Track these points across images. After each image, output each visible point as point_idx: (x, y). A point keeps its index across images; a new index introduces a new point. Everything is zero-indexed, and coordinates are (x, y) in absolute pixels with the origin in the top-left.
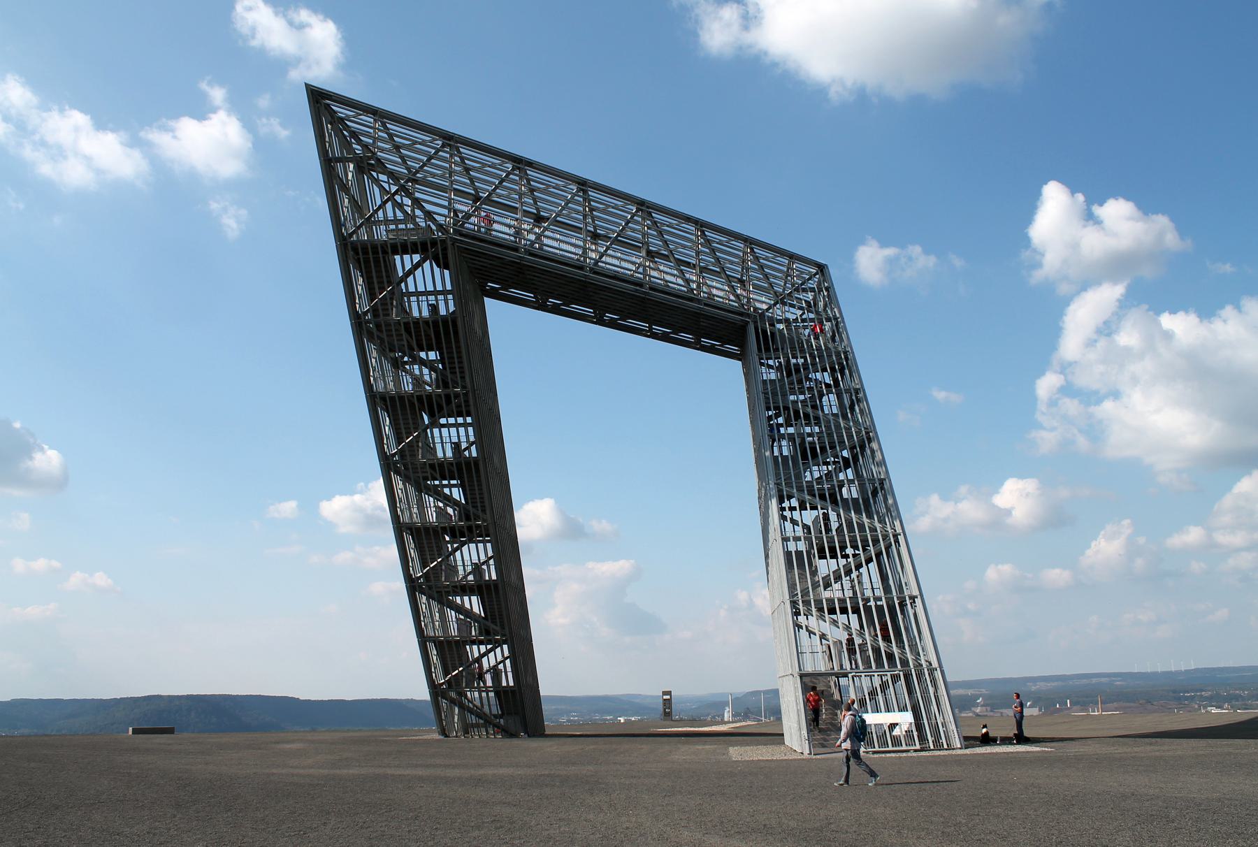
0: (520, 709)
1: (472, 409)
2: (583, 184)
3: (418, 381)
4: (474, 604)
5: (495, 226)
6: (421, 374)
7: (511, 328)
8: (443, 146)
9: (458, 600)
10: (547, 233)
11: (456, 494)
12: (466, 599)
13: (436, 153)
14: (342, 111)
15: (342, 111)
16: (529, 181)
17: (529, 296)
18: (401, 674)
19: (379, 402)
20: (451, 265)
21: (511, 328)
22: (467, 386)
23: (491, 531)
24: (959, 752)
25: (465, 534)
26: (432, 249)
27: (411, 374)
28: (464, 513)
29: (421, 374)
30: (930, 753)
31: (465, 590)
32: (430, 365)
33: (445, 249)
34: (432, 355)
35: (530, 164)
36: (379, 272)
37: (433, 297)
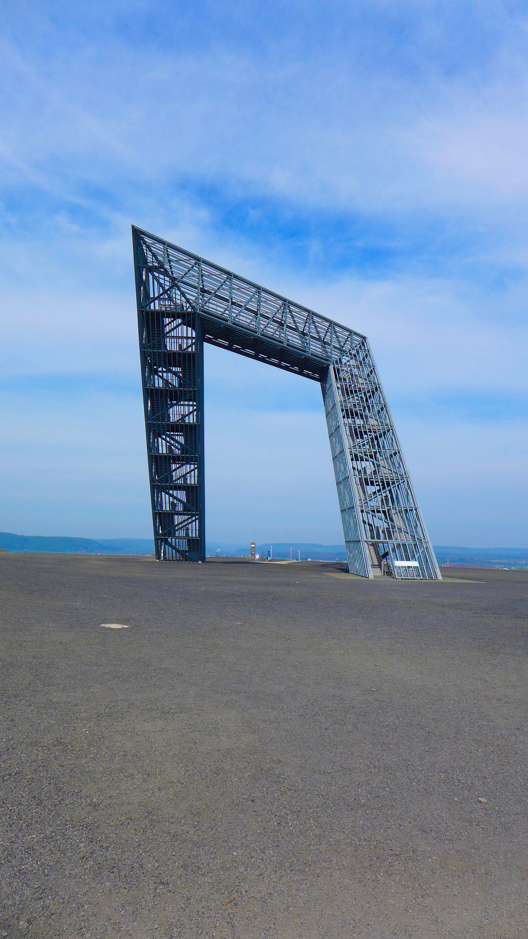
0: (196, 548)
1: (197, 399)
2: (258, 288)
3: (166, 382)
4: (182, 495)
5: (311, 347)
6: (169, 378)
7: (217, 360)
8: (196, 264)
9: (171, 492)
10: (211, 301)
11: (181, 439)
12: (175, 491)
13: (192, 267)
14: (148, 241)
15: (148, 241)
16: (168, 255)
17: (226, 343)
18: (140, 526)
19: (150, 393)
20: (196, 327)
21: (217, 360)
22: (192, 388)
23: (198, 460)
24: (429, 581)
25: (182, 460)
26: (189, 319)
27: (162, 377)
28: (183, 449)
29: (169, 378)
30: (434, 581)
31: (178, 488)
32: (175, 373)
33: (194, 318)
34: (179, 369)
35: (236, 277)
36: (153, 325)
37: (180, 340)
